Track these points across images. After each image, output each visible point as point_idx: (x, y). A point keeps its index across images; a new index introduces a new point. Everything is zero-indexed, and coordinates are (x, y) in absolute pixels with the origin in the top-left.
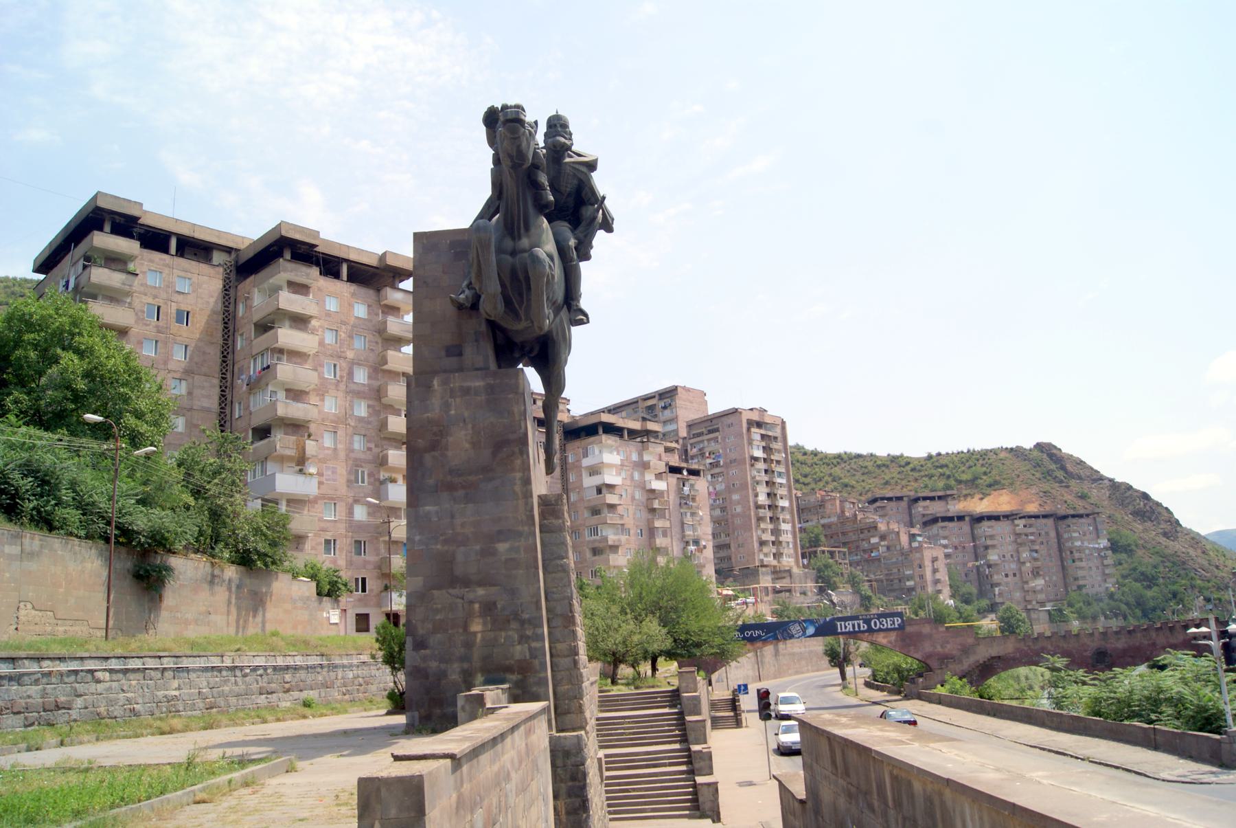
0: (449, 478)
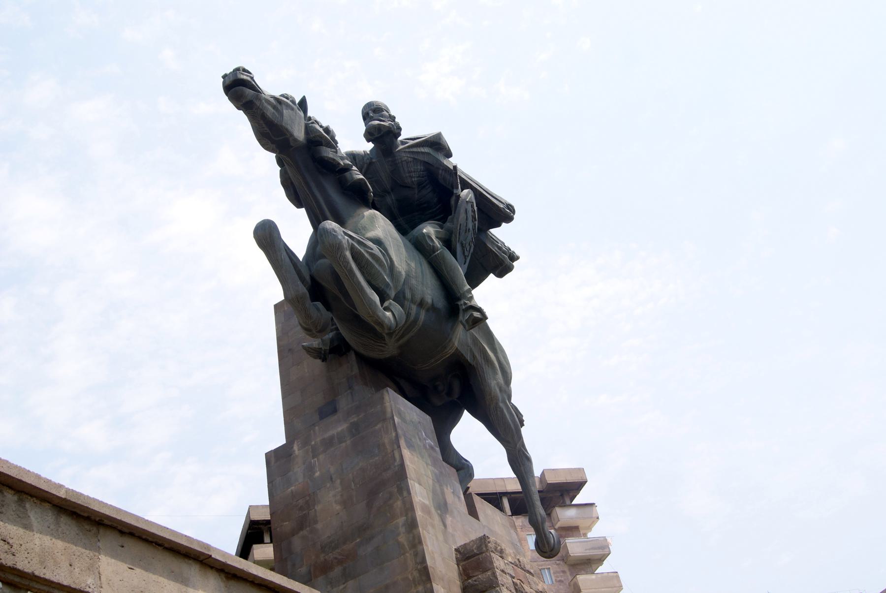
0: (322, 557)
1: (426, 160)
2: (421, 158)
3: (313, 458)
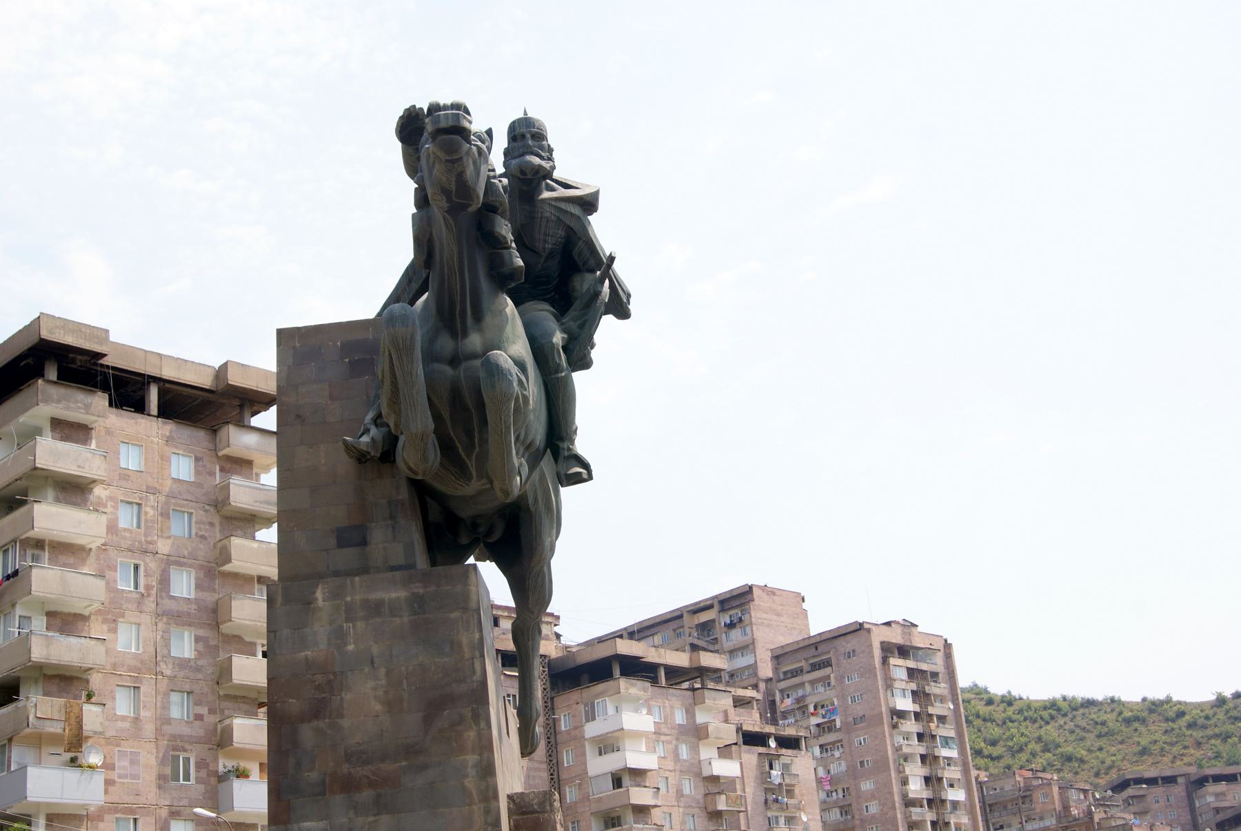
0: (345, 768)
1: (572, 225)
2: (567, 220)
3: (346, 621)
